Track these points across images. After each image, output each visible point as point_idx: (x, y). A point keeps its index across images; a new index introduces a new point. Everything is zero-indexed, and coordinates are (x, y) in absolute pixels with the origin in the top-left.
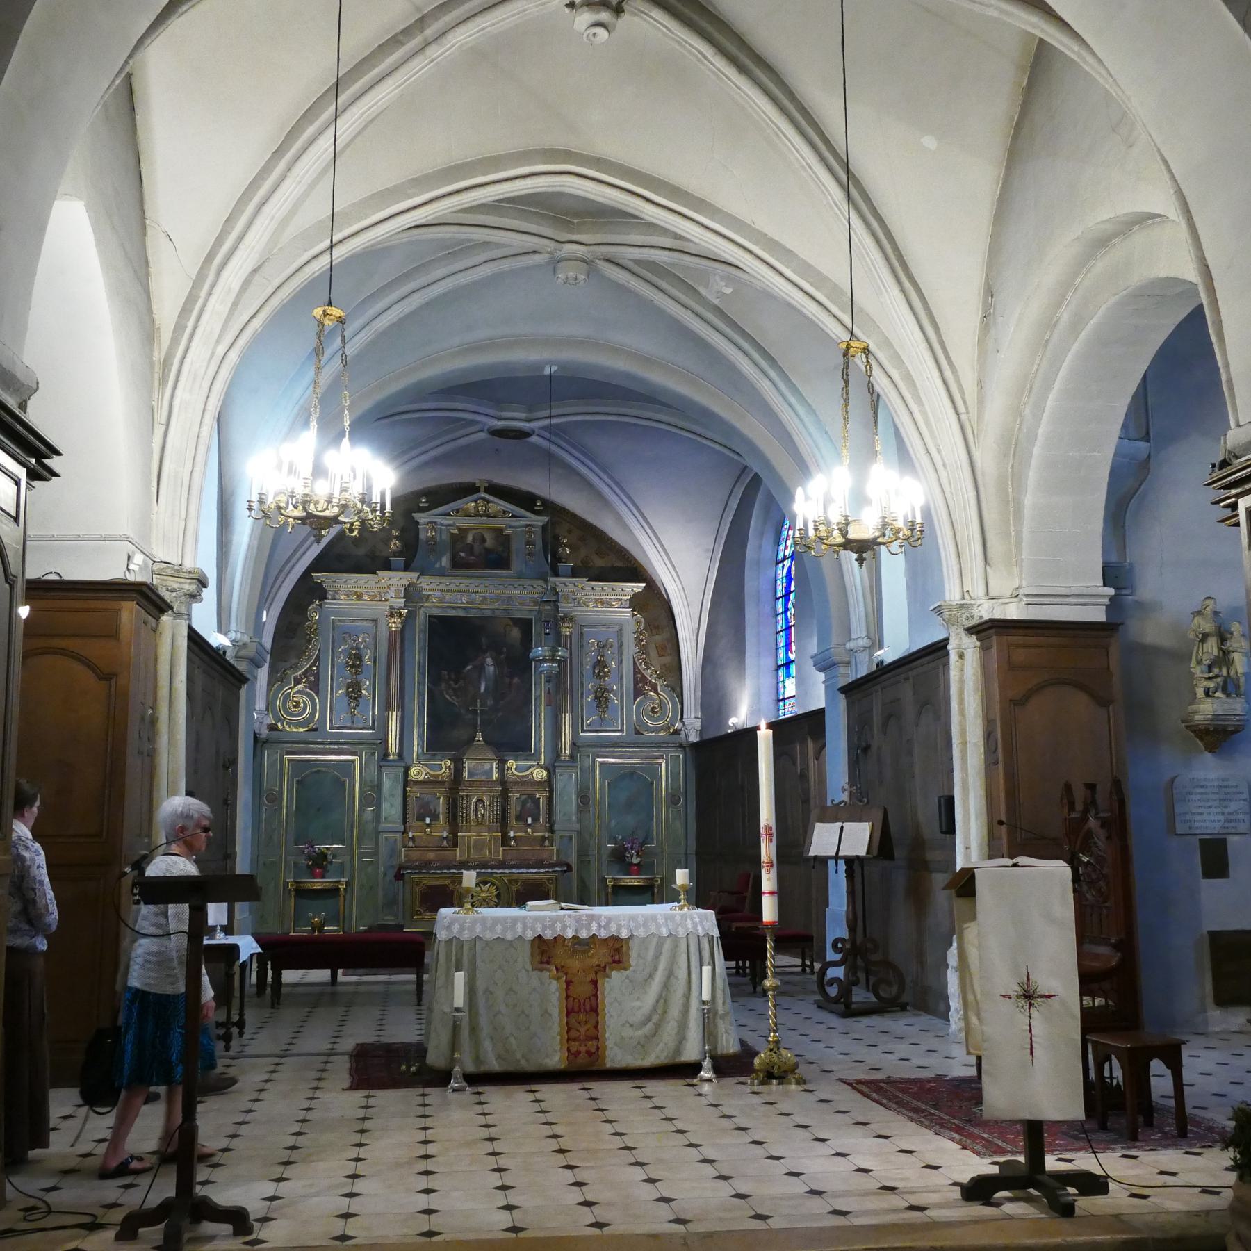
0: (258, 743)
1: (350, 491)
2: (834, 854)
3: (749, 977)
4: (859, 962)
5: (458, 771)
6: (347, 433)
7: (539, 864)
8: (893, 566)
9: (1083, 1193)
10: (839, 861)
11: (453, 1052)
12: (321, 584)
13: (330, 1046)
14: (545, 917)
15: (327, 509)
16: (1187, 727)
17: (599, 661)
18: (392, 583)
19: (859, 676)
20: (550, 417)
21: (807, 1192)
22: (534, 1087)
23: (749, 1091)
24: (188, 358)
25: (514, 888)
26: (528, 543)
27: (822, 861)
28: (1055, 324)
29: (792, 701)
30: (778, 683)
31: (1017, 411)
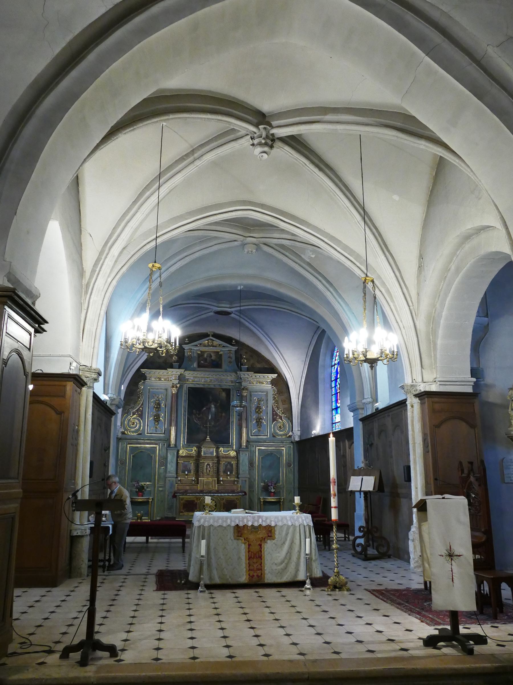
0: (119, 440)
1: (162, 338)
2: (359, 490)
3: (322, 542)
4: (370, 536)
6: (161, 314)
7: (233, 492)
8: (382, 368)
9: (476, 643)
10: (361, 493)
11: (200, 575)
13: (147, 571)
14: (239, 517)
15: (153, 345)
16: (508, 437)
18: (173, 374)
19: (368, 414)
20: (240, 306)
21: (356, 641)
22: (235, 591)
23: (327, 594)
24: (96, 283)
25: (222, 502)
26: (230, 357)
27: (353, 493)
28: (449, 270)
29: (338, 424)
30: (332, 416)
31: (433, 306)
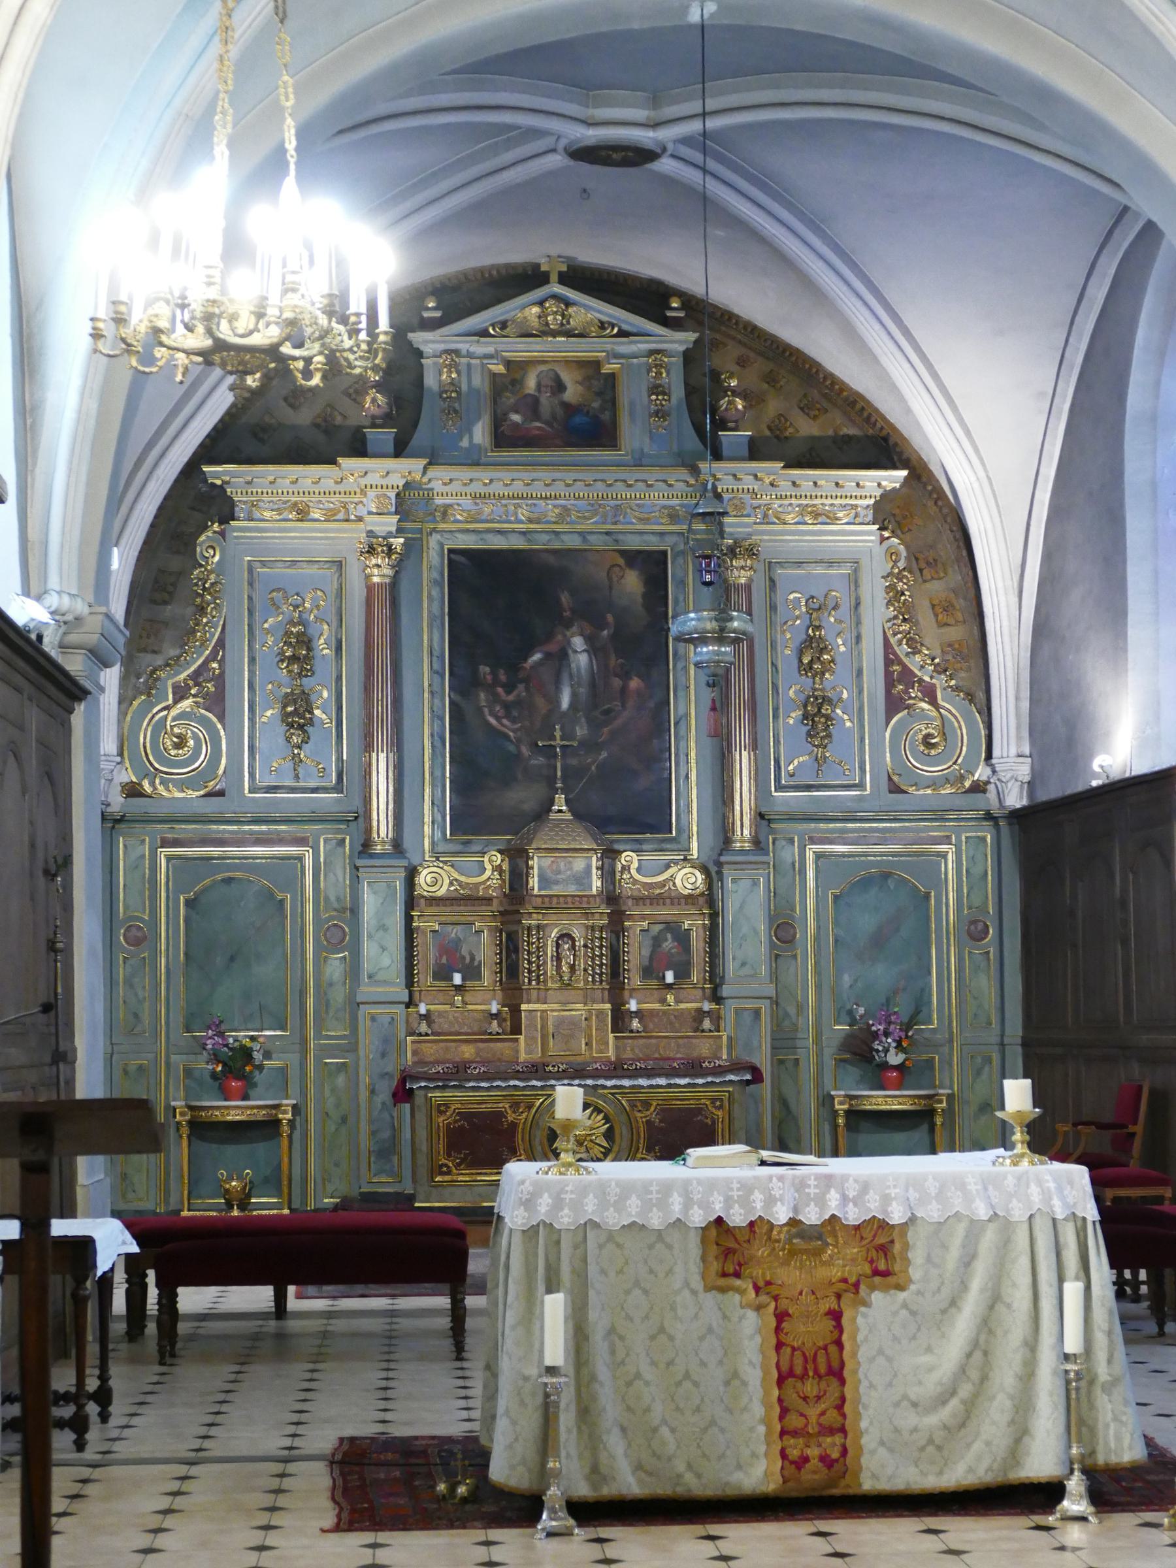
0: (113, 823)
1: (302, 290)
5: (517, 878)
6: (292, 167)
7: (693, 1067)
12: (221, 488)
14: (728, 1181)
15: (257, 330)
17: (810, 639)
20: (704, 115)
22: (714, 1529)
26: (656, 389)
